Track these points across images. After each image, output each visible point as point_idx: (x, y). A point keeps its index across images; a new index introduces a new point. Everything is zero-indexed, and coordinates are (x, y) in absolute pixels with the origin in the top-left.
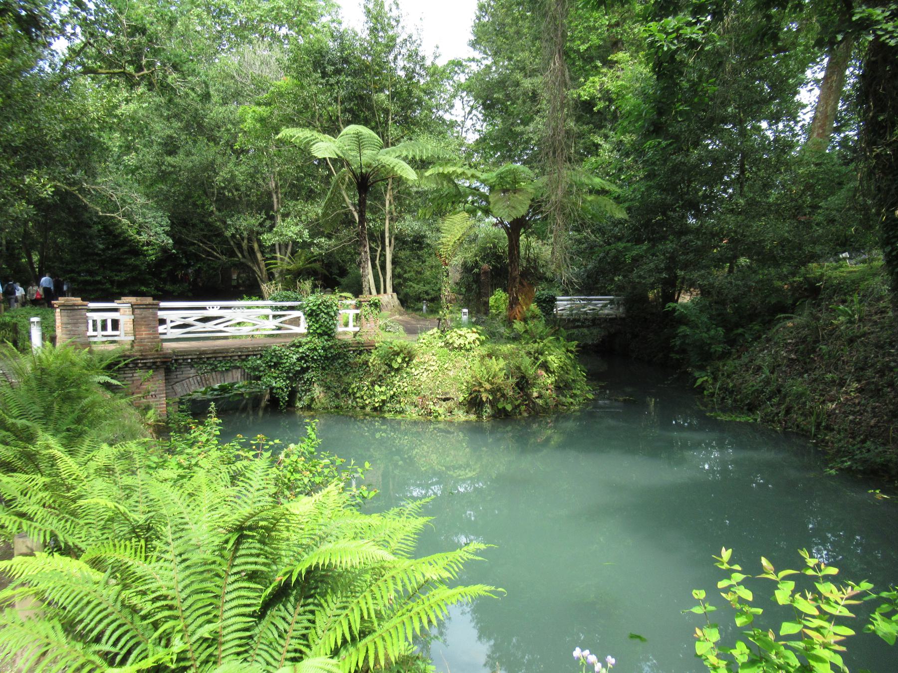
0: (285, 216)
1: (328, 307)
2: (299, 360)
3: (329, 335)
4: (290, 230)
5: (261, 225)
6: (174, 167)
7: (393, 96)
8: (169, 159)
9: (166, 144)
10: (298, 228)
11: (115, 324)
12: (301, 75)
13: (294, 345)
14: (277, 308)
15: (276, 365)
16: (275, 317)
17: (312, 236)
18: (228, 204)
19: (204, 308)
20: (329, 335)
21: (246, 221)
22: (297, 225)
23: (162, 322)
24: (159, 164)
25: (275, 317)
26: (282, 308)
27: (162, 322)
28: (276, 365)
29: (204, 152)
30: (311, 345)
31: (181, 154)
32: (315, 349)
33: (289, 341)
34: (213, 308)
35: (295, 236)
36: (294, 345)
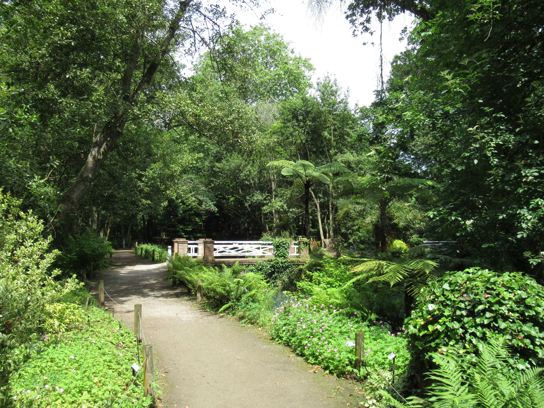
0: (276, 196)
1: (284, 244)
2: (271, 267)
3: (284, 257)
4: (277, 204)
5: (265, 199)
6: (219, 168)
7: (249, 205)
8: (217, 164)
9: (216, 156)
10: (282, 203)
11: (196, 250)
12: (286, 121)
13: (269, 261)
14: (263, 244)
15: (261, 270)
16: (262, 248)
17: (289, 208)
18: (247, 188)
19: (232, 244)
20: (284, 257)
21: (258, 197)
22: (281, 201)
23: (215, 250)
24: (212, 167)
25: (262, 248)
26: (265, 244)
27: (215, 250)
28: (261, 270)
29: (234, 161)
30: (276, 261)
31: (224, 161)
32: (278, 263)
33: (266, 259)
34: (236, 244)
35: (279, 208)
36: (269, 261)
